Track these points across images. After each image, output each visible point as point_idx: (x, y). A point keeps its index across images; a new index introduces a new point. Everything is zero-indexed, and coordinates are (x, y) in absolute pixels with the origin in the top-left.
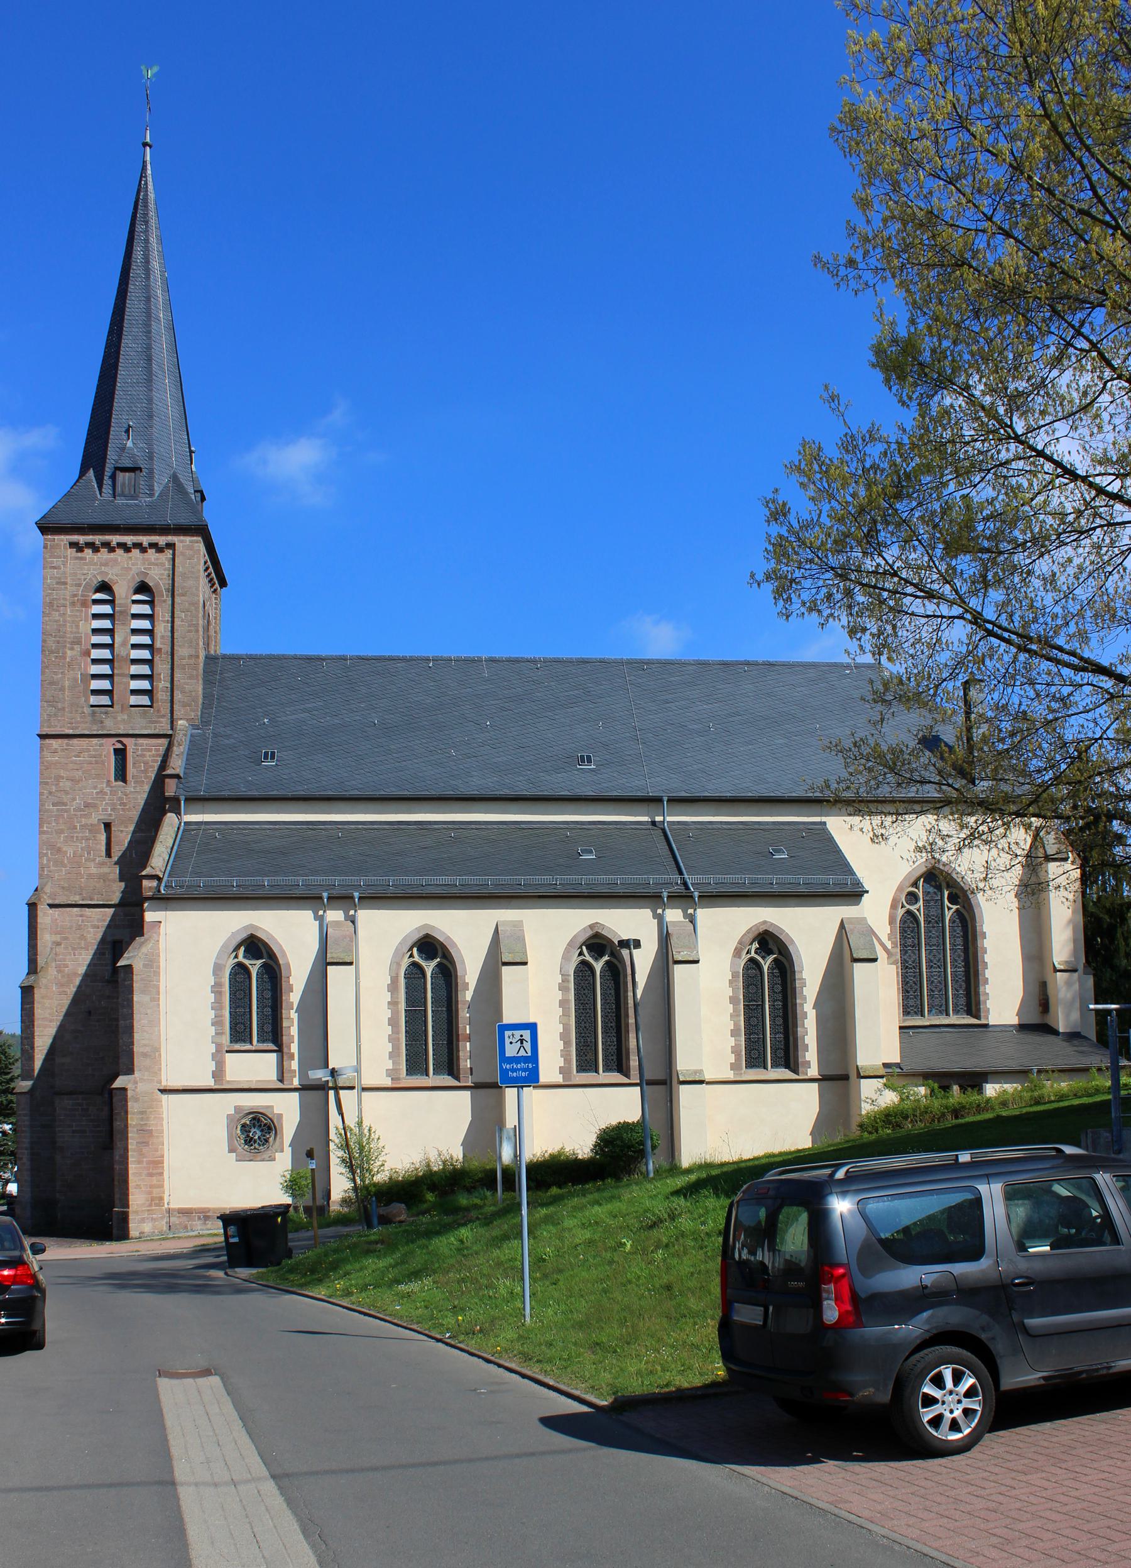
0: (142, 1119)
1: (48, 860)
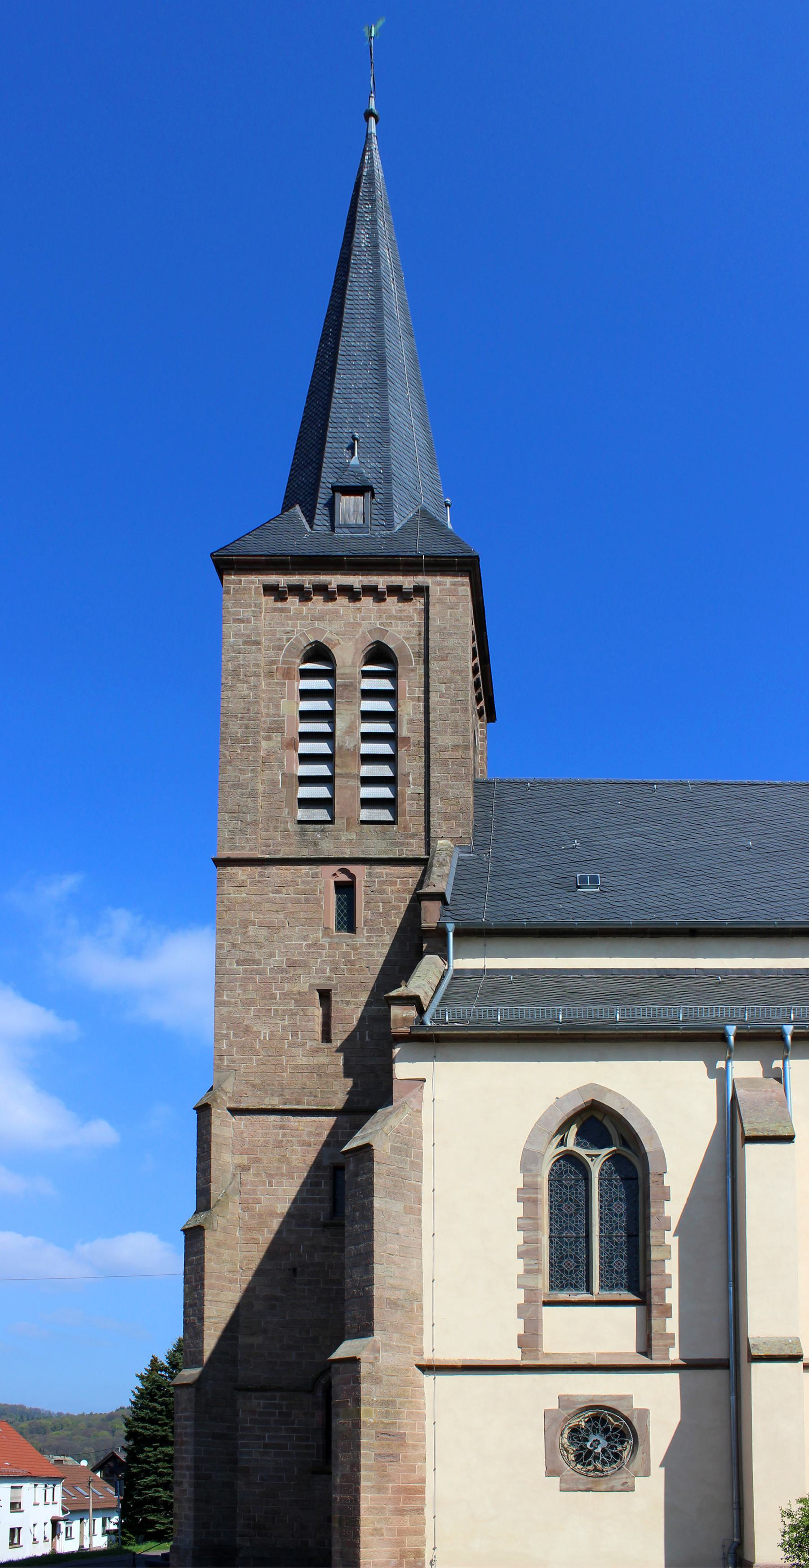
0: (387, 1414)
1: (230, 1045)
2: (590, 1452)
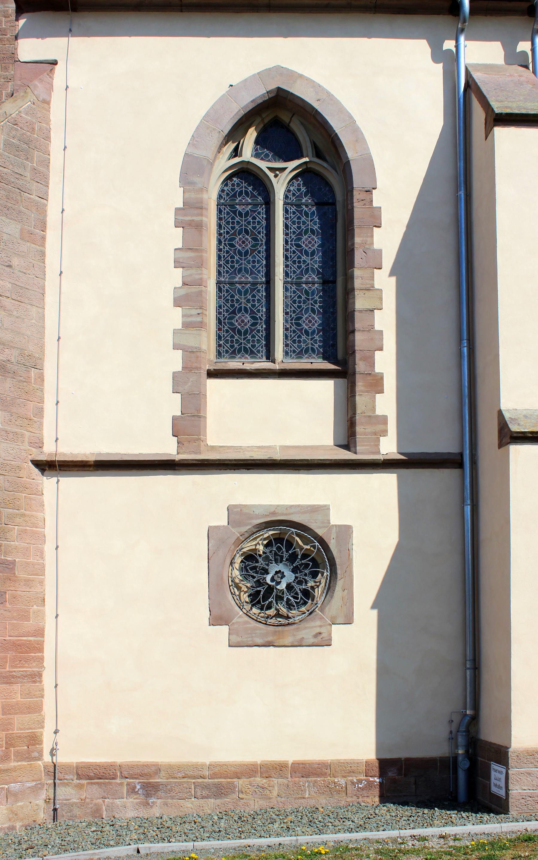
2: (270, 589)
